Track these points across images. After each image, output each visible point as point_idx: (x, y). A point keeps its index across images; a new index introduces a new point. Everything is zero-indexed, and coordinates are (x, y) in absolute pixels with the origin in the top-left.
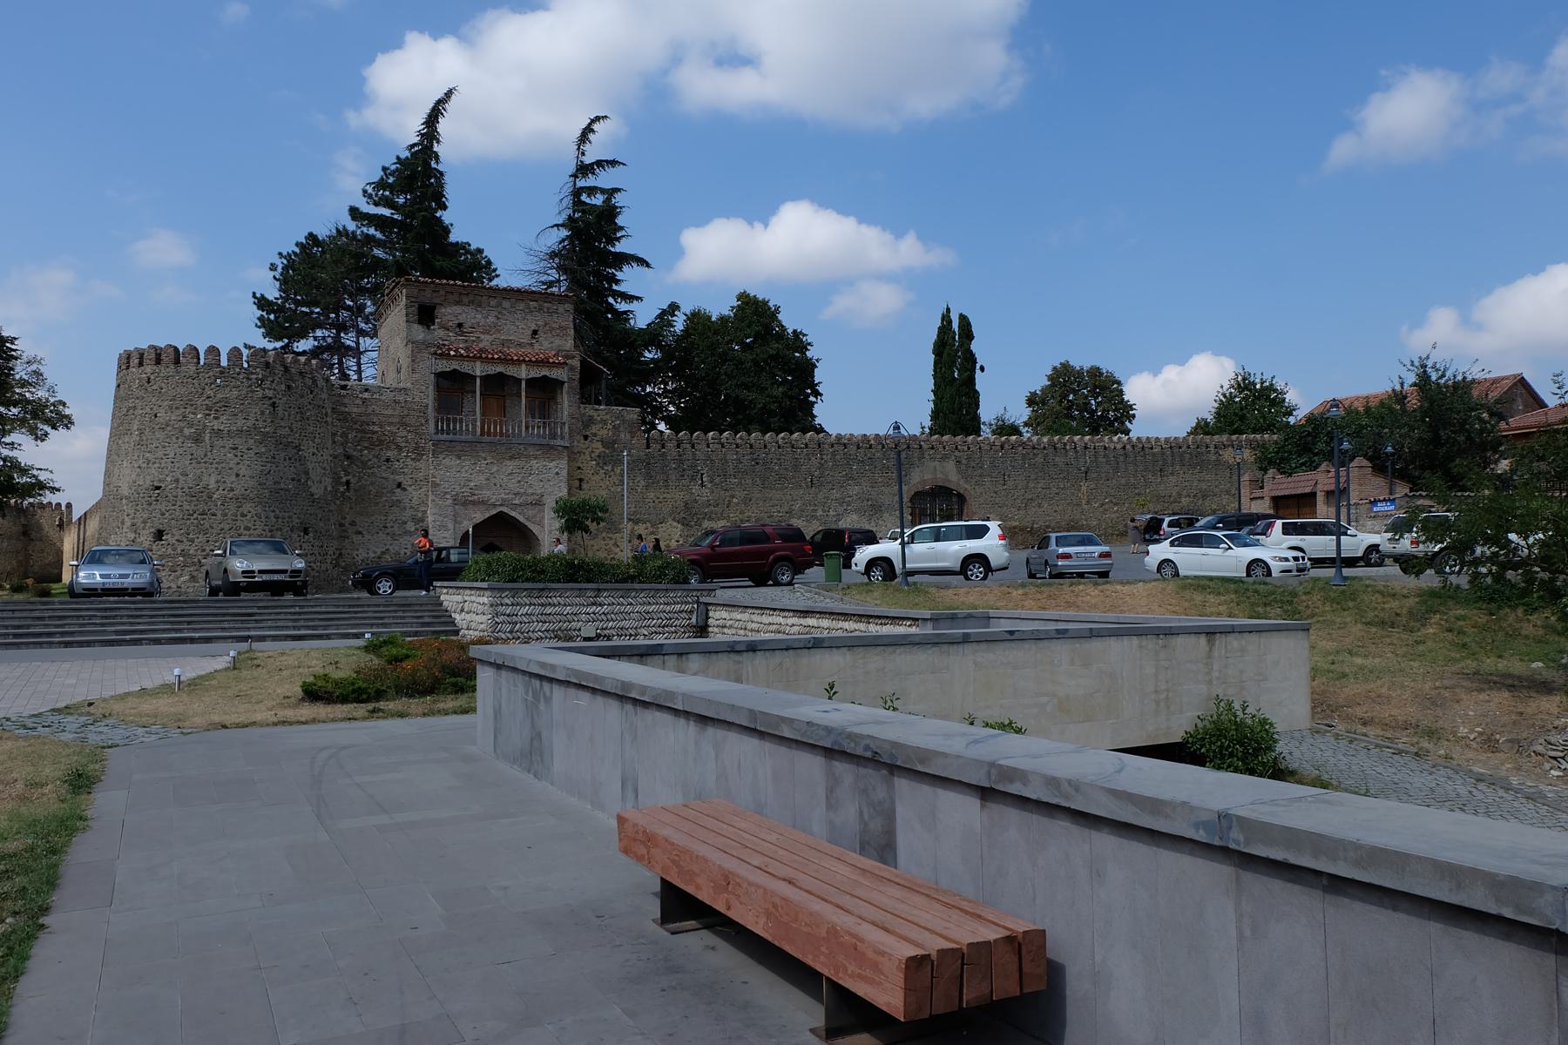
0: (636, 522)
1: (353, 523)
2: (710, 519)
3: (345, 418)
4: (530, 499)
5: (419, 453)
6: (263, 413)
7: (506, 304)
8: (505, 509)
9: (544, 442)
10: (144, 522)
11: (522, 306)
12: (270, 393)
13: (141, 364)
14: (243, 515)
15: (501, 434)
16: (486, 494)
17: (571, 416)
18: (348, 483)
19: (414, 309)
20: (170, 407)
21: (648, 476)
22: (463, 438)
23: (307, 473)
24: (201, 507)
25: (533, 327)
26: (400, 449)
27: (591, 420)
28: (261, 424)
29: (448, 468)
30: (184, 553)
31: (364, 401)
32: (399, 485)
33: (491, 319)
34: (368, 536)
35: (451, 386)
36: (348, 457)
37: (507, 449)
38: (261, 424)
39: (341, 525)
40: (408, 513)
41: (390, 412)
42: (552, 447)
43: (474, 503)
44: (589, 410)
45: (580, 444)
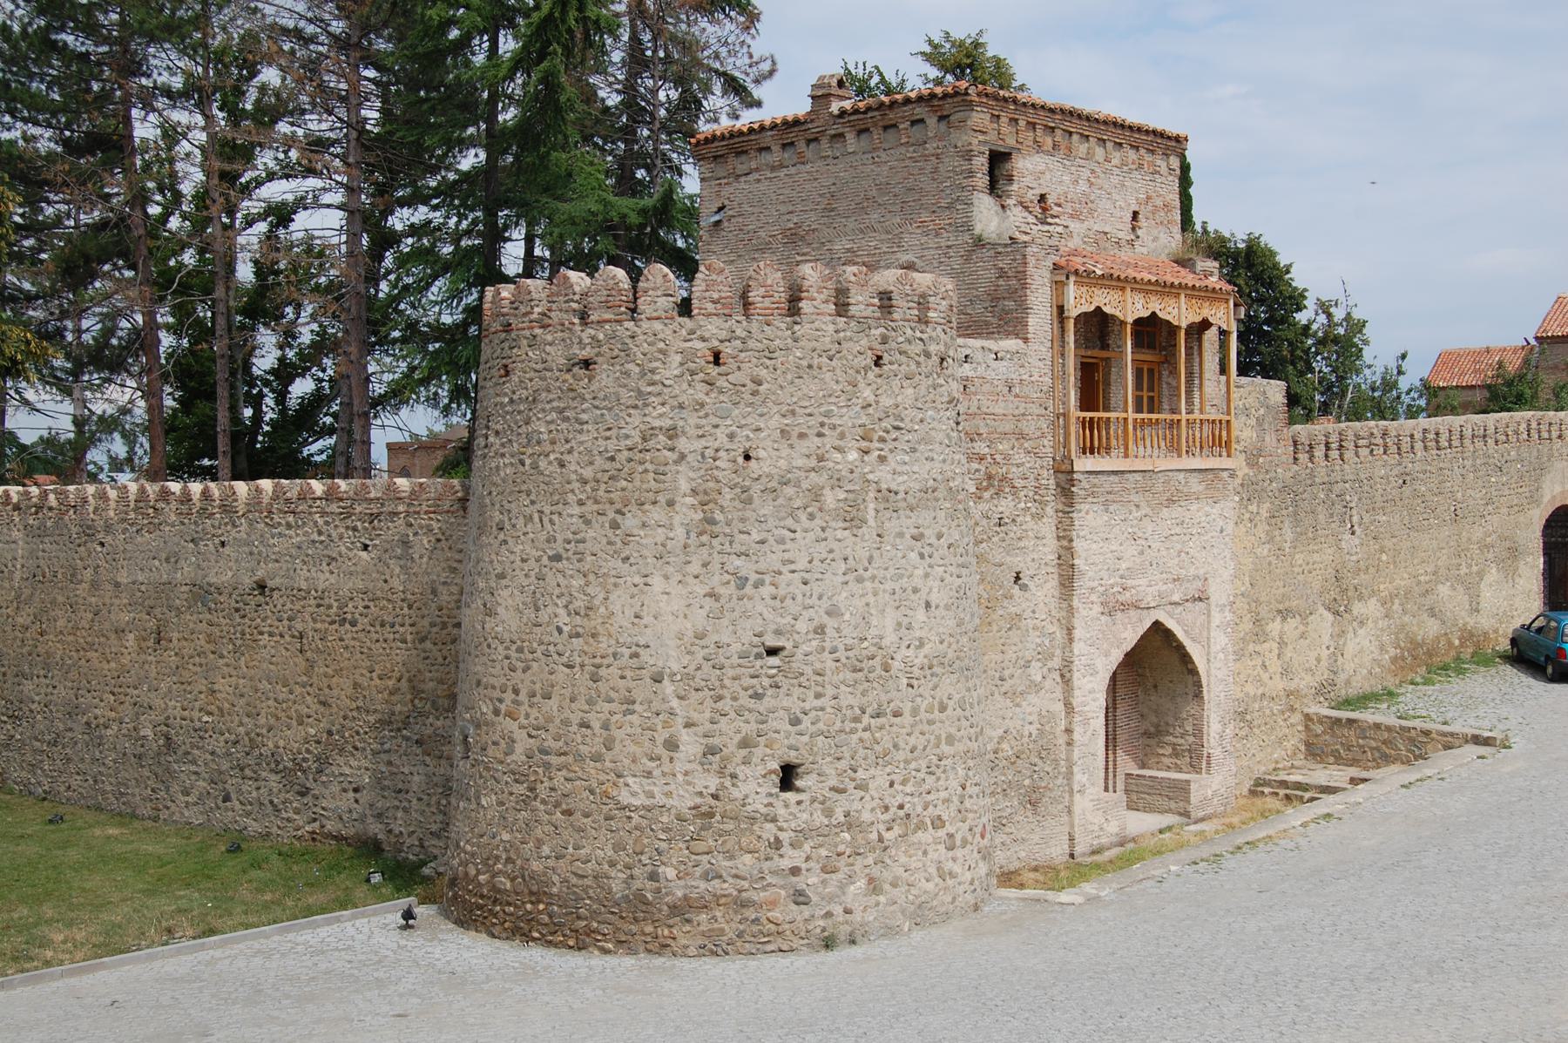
24: (876, 696)
30: (851, 823)
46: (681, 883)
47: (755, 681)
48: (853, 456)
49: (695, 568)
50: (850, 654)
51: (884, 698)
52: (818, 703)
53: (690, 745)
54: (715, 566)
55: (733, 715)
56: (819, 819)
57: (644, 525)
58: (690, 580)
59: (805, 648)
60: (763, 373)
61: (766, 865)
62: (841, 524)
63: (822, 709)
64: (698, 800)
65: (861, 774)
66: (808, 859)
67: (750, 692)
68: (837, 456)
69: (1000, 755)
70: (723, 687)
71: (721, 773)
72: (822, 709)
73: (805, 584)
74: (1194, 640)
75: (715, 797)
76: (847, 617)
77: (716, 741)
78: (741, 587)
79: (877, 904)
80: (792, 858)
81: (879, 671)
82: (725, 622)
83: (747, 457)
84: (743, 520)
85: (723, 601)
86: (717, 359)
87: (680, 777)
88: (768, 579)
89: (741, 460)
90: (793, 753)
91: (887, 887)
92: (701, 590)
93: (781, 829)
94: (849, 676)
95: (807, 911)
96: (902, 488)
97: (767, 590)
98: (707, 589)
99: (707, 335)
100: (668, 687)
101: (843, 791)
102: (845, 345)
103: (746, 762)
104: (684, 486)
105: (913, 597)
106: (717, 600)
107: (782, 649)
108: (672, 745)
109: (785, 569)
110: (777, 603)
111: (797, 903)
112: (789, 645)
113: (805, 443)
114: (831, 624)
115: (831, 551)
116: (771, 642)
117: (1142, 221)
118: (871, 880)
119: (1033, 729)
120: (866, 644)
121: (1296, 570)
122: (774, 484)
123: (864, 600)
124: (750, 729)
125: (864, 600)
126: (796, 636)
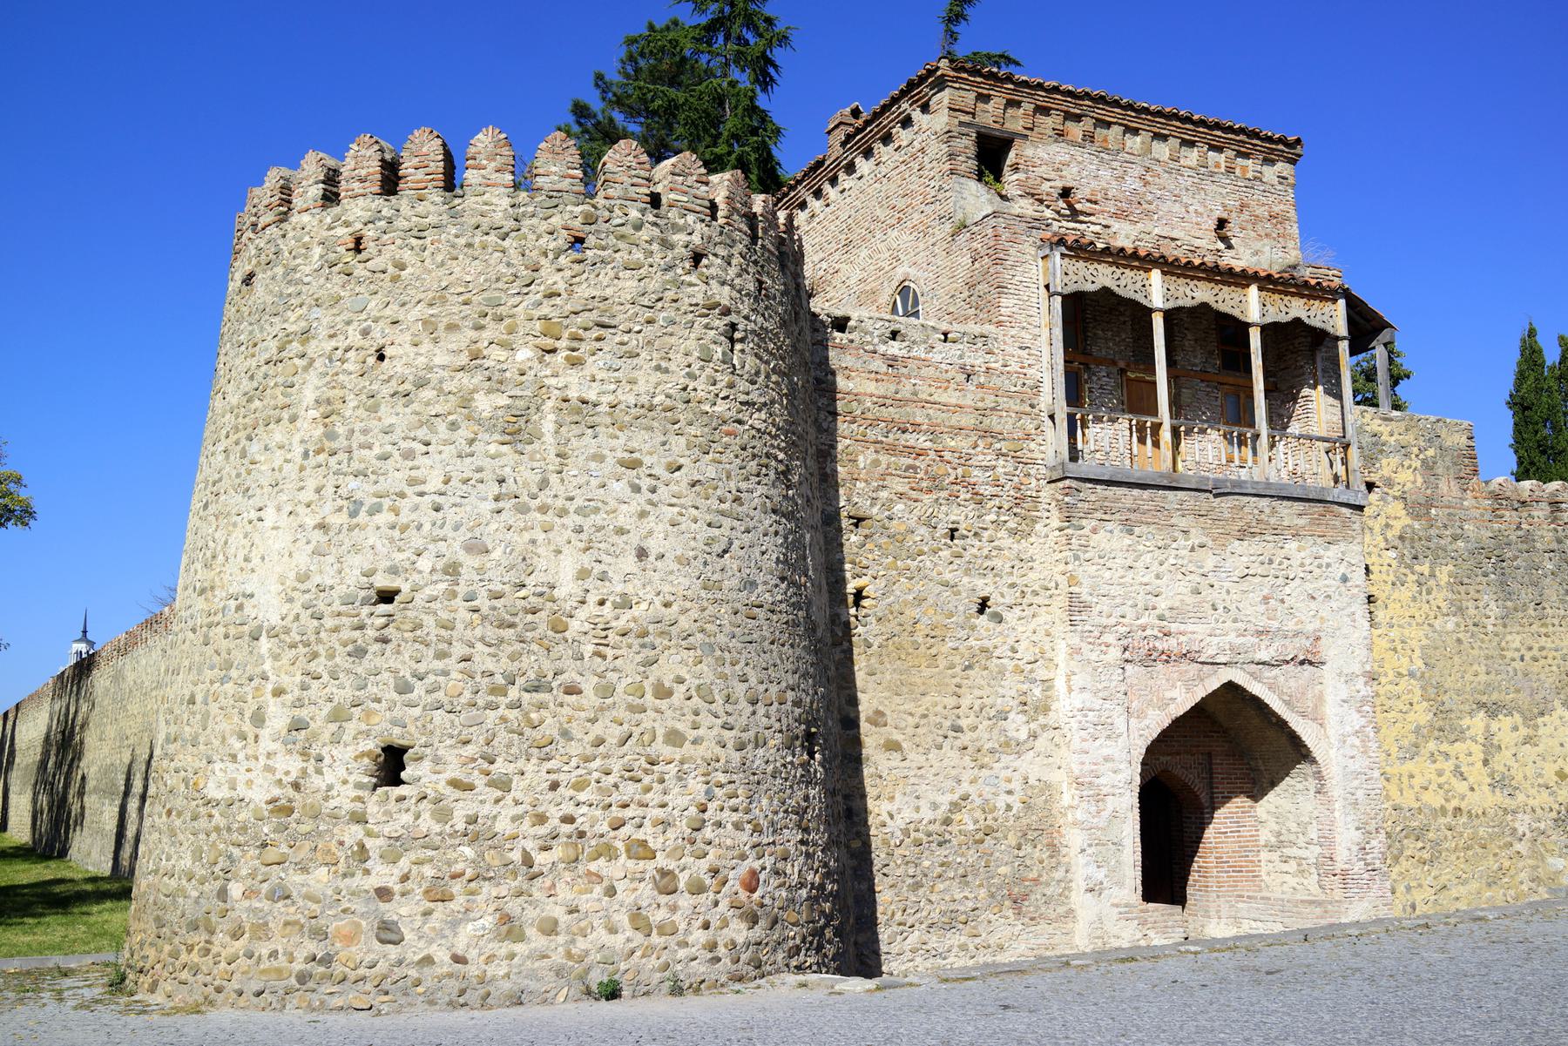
0: (1493, 710)
10: (338, 716)
13: (330, 198)
14: (663, 693)
20: (429, 325)
24: (533, 663)
25: (1219, 213)
30: (475, 831)
31: (892, 362)
33: (1132, 183)
34: (915, 758)
40: (1011, 686)
41: (951, 397)
46: (246, 903)
47: (357, 634)
48: (524, 354)
49: (307, 495)
50: (498, 603)
51: (548, 667)
52: (439, 665)
53: (278, 717)
54: (330, 490)
55: (326, 677)
56: (427, 823)
57: (266, 449)
58: (301, 510)
59: (429, 591)
60: (407, 255)
61: (343, 884)
62: (497, 437)
63: (446, 673)
64: (277, 792)
65: (500, 767)
66: (405, 878)
67: (350, 648)
68: (501, 354)
69: (954, 828)
70: (319, 641)
71: (304, 754)
72: (446, 673)
73: (437, 510)
74: (1303, 715)
75: (296, 786)
76: (497, 554)
77: (304, 713)
78: (353, 514)
79: (512, 956)
80: (382, 874)
81: (543, 628)
82: (330, 559)
83: (381, 358)
84: (365, 432)
85: (331, 533)
86: (358, 247)
87: (262, 760)
88: (387, 503)
89: (372, 360)
90: (397, 731)
91: (531, 932)
92: (310, 521)
93: (369, 834)
94: (491, 633)
95: (393, 952)
96: (605, 399)
97: (384, 518)
98: (318, 520)
99: (351, 219)
100: (265, 644)
101: (470, 787)
102: (526, 222)
103: (336, 740)
104: (309, 396)
105: (615, 539)
106: (326, 533)
107: (397, 592)
108: (259, 719)
109: (409, 491)
110: (396, 533)
111: (383, 942)
112: (406, 588)
113: (454, 337)
114: (469, 562)
115: (479, 470)
116: (382, 582)
117: (1232, 230)
118: (506, 919)
119: (1015, 801)
120: (523, 593)
121: (1509, 654)
122: (407, 386)
123: (527, 536)
124: (344, 694)
125: (527, 536)
126: (416, 577)
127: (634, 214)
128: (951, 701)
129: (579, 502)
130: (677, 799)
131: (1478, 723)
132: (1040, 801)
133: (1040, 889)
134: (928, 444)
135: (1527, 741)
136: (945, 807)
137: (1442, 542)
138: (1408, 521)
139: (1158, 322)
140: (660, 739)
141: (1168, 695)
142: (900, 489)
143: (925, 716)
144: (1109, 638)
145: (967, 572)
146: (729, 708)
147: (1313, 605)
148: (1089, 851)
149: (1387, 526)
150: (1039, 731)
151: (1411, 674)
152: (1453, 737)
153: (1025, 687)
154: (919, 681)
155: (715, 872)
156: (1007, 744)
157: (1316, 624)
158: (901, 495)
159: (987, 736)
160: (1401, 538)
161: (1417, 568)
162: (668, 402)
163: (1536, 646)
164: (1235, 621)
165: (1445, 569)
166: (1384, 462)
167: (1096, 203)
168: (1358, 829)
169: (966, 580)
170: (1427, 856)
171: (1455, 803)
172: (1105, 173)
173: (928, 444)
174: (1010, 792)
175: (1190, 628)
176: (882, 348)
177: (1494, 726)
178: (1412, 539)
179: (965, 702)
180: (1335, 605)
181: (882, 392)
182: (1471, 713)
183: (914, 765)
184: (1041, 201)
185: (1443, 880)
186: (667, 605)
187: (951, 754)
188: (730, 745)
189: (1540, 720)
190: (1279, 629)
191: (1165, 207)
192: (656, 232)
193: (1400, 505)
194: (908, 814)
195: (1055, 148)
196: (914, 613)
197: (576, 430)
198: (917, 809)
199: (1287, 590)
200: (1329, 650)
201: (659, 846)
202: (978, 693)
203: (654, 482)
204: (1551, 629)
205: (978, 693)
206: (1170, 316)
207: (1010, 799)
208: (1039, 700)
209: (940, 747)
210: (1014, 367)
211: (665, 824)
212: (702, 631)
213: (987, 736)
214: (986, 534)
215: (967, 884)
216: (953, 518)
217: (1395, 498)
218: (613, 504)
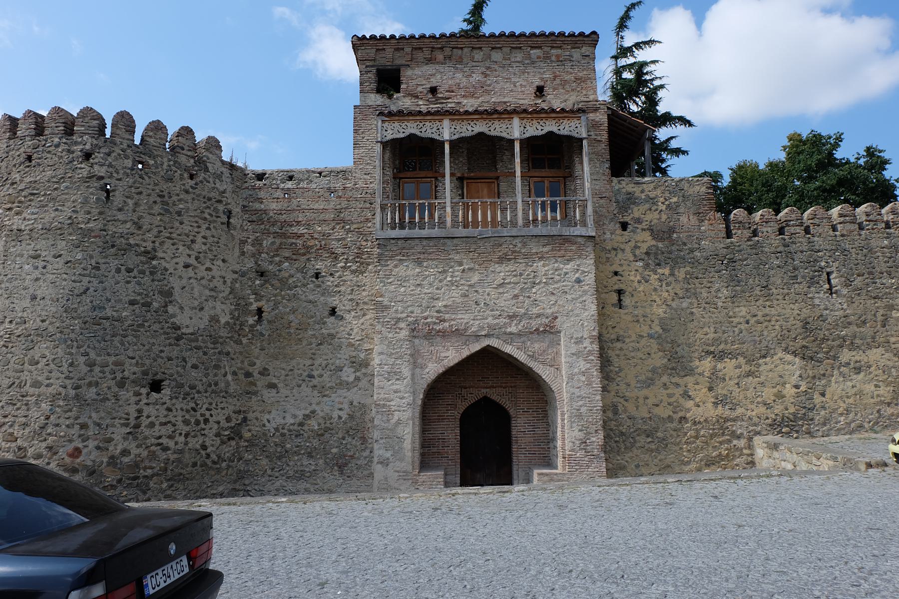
0: (720, 356)
1: (264, 372)
2: (853, 347)
3: (258, 218)
4: (535, 324)
5: (361, 260)
6: (86, 202)
7: (497, 56)
8: (494, 343)
9: (554, 231)
11: (518, 56)
12: (101, 171)
15: (485, 223)
16: (462, 318)
17: (598, 195)
18: (260, 311)
19: (372, 76)
21: (734, 280)
22: (425, 233)
23: (168, 294)
25: (538, 82)
26: (335, 257)
27: (631, 200)
28: (81, 217)
29: (403, 280)
32: (333, 312)
33: (477, 77)
35: (411, 160)
36: (262, 274)
37: (498, 248)
38: (81, 217)
39: (248, 375)
42: (566, 240)
43: (444, 334)
44: (626, 185)
45: (614, 236)
69: (306, 428)
121: (736, 320)
127: (56, 140)
128: (309, 362)
129: (9, 276)
130: (34, 413)
131: (707, 364)
132: (358, 414)
133: (354, 461)
134: (306, 231)
135: (749, 374)
136: (301, 417)
137: (682, 254)
138: (654, 243)
139: (447, 147)
140: (28, 385)
141: (443, 355)
142: (287, 255)
143: (291, 370)
144: (402, 325)
145: (323, 294)
146: (71, 369)
147: (553, 298)
148: (381, 442)
149: (636, 247)
150: (362, 376)
151: (650, 336)
152: (682, 373)
153: (354, 354)
154: (290, 352)
155: (50, 448)
156: (341, 384)
157: (555, 309)
158: (287, 258)
159: (328, 380)
160: (647, 253)
161: (660, 271)
162: (60, 225)
163: (760, 313)
164: (492, 310)
165: (683, 270)
166: (636, 209)
167: (453, 92)
168: (580, 430)
169: (322, 298)
170: (653, 447)
171: (681, 414)
172: (459, 75)
173: (306, 231)
174: (341, 409)
175: (460, 316)
176: (282, 185)
177: (719, 366)
178: (656, 254)
179: (317, 363)
180: (569, 297)
181: (280, 207)
182: (700, 359)
183: (283, 396)
184: (417, 97)
185: (668, 462)
186: (43, 321)
187: (307, 389)
188: (69, 387)
189: (761, 361)
190: (525, 314)
191: (498, 86)
192: (66, 147)
193: (648, 233)
194: (279, 421)
195: (426, 68)
196: (291, 317)
197: (13, 243)
198: (284, 418)
199: (534, 290)
200: (564, 325)
201: (20, 435)
202: (324, 357)
203: (45, 263)
204: (775, 302)
205: (324, 357)
206: (522, 141)
207: (341, 413)
208: (363, 360)
209: (299, 386)
210: (361, 184)
211: (25, 425)
212: (61, 332)
213: (328, 380)
214: (337, 274)
215: (312, 457)
216: (318, 267)
217: (643, 230)
218: (24, 275)
